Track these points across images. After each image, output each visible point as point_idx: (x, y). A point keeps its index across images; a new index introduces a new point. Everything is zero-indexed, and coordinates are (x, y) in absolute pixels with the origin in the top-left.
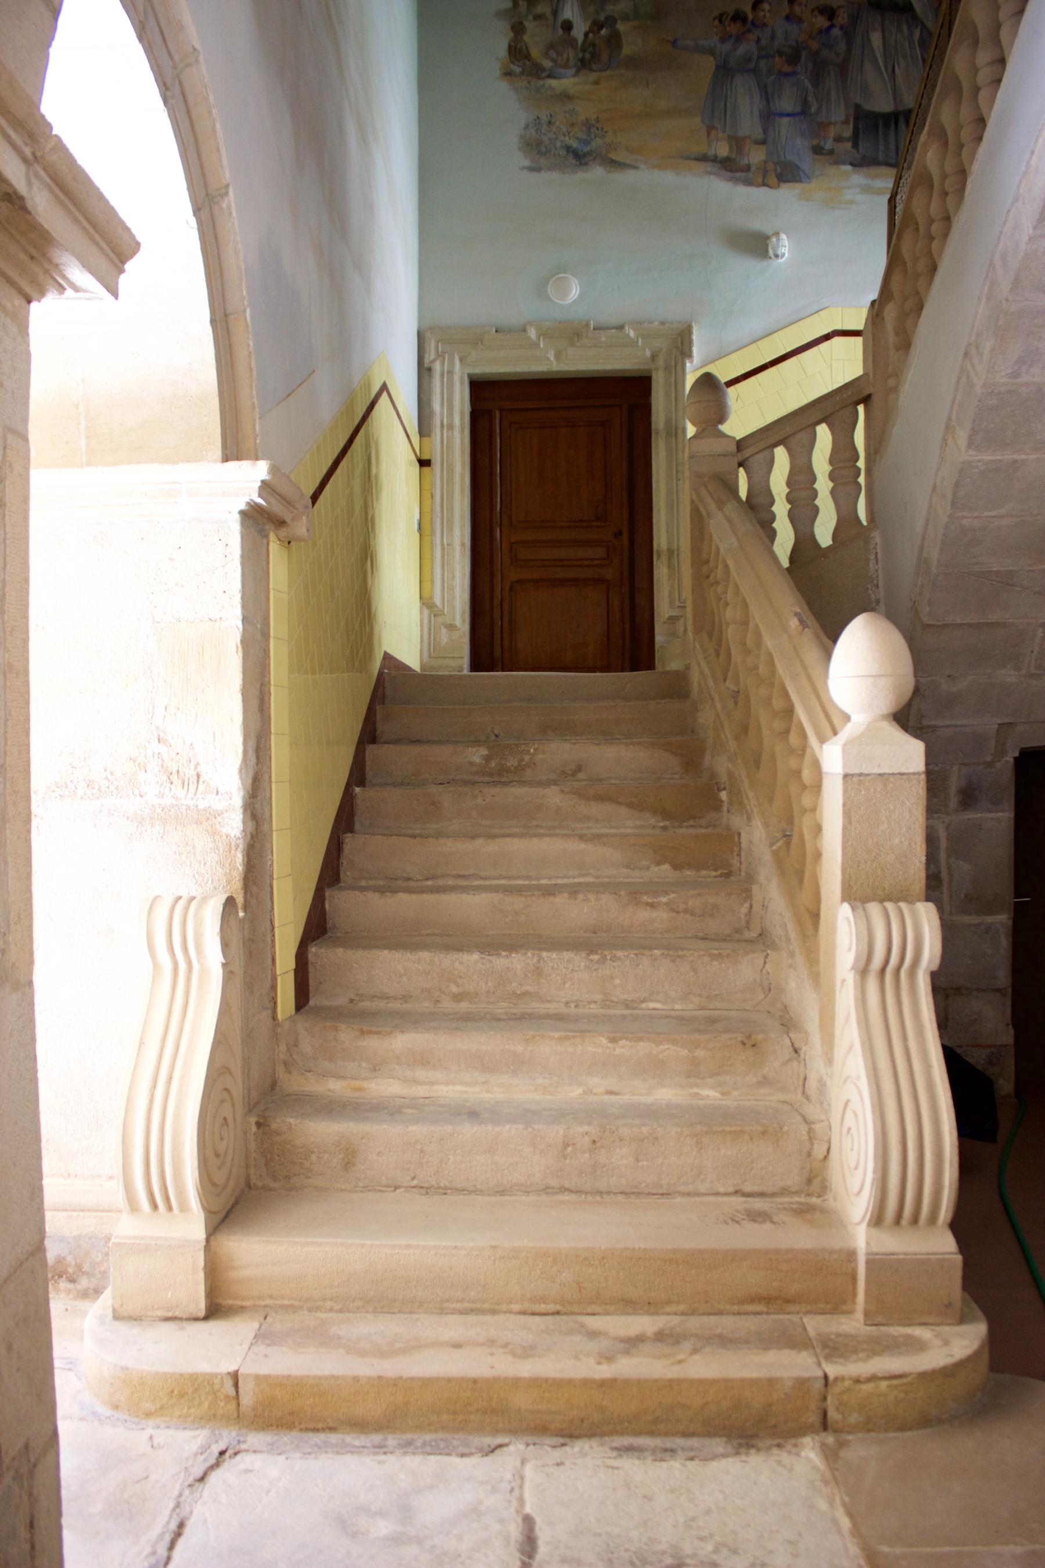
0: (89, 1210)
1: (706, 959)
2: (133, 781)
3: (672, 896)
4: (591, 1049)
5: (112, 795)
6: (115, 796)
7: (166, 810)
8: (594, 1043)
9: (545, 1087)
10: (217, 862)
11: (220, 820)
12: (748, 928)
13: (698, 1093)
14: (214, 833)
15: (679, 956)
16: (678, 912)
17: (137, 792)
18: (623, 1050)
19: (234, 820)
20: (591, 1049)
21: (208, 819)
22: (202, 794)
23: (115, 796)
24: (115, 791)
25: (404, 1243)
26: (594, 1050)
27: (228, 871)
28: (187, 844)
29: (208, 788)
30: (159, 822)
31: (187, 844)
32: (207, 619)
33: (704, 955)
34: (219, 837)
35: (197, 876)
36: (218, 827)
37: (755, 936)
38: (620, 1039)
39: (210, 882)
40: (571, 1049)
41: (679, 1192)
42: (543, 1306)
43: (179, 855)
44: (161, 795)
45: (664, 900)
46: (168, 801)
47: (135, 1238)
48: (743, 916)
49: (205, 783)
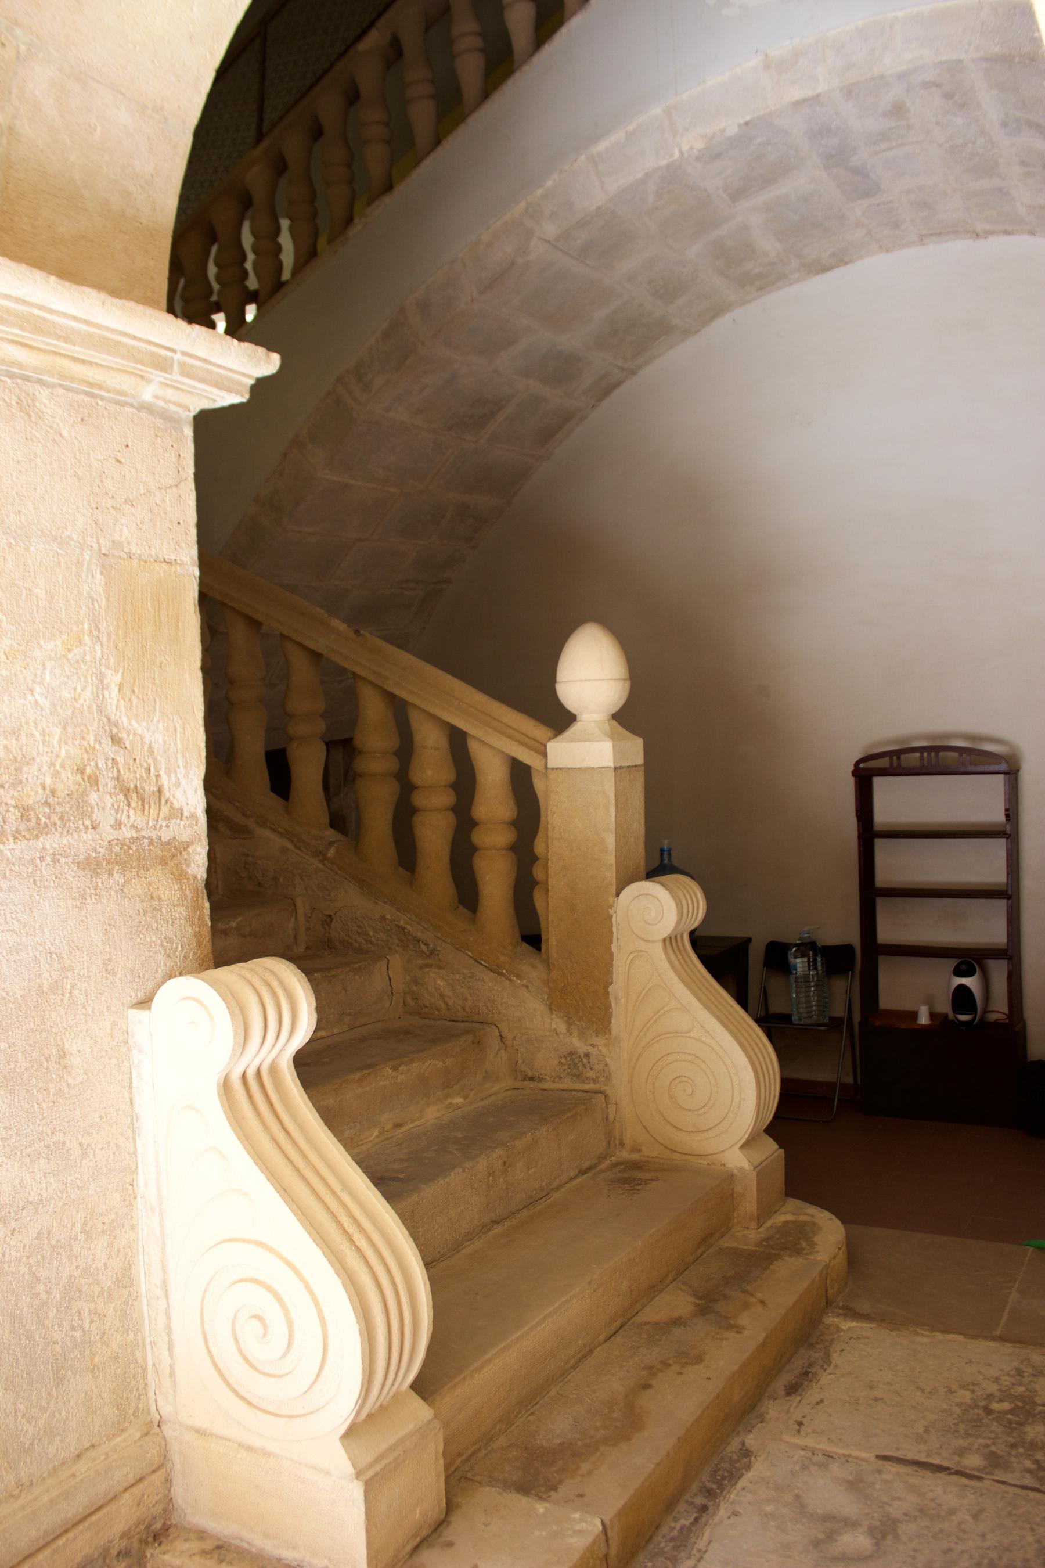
0: (75, 1525)
1: (351, 974)
2: (81, 804)
3: (239, 919)
4: (381, 1083)
5: (56, 829)
6: (60, 830)
7: (126, 848)
8: (383, 1076)
9: (352, 1139)
10: (186, 919)
11: (185, 857)
12: (296, 943)
13: (451, 1103)
14: (180, 876)
15: (333, 976)
16: (245, 936)
17: (88, 823)
18: (403, 1077)
19: (199, 854)
20: (381, 1083)
21: (173, 856)
22: (165, 819)
23: (60, 830)
24: (59, 823)
25: (542, 1316)
26: (383, 1083)
27: (197, 929)
28: (152, 897)
29: (172, 811)
30: (117, 868)
31: (152, 897)
32: (162, 560)
33: (350, 971)
34: (186, 881)
35: (165, 944)
36: (184, 866)
37: (303, 950)
38: (400, 1066)
39: (180, 948)
40: (368, 1089)
41: (552, 1189)
42: (615, 1324)
43: (144, 915)
44: (118, 825)
45: (233, 924)
46: (127, 833)
47: (377, 1461)
48: (291, 932)
49: (169, 804)
